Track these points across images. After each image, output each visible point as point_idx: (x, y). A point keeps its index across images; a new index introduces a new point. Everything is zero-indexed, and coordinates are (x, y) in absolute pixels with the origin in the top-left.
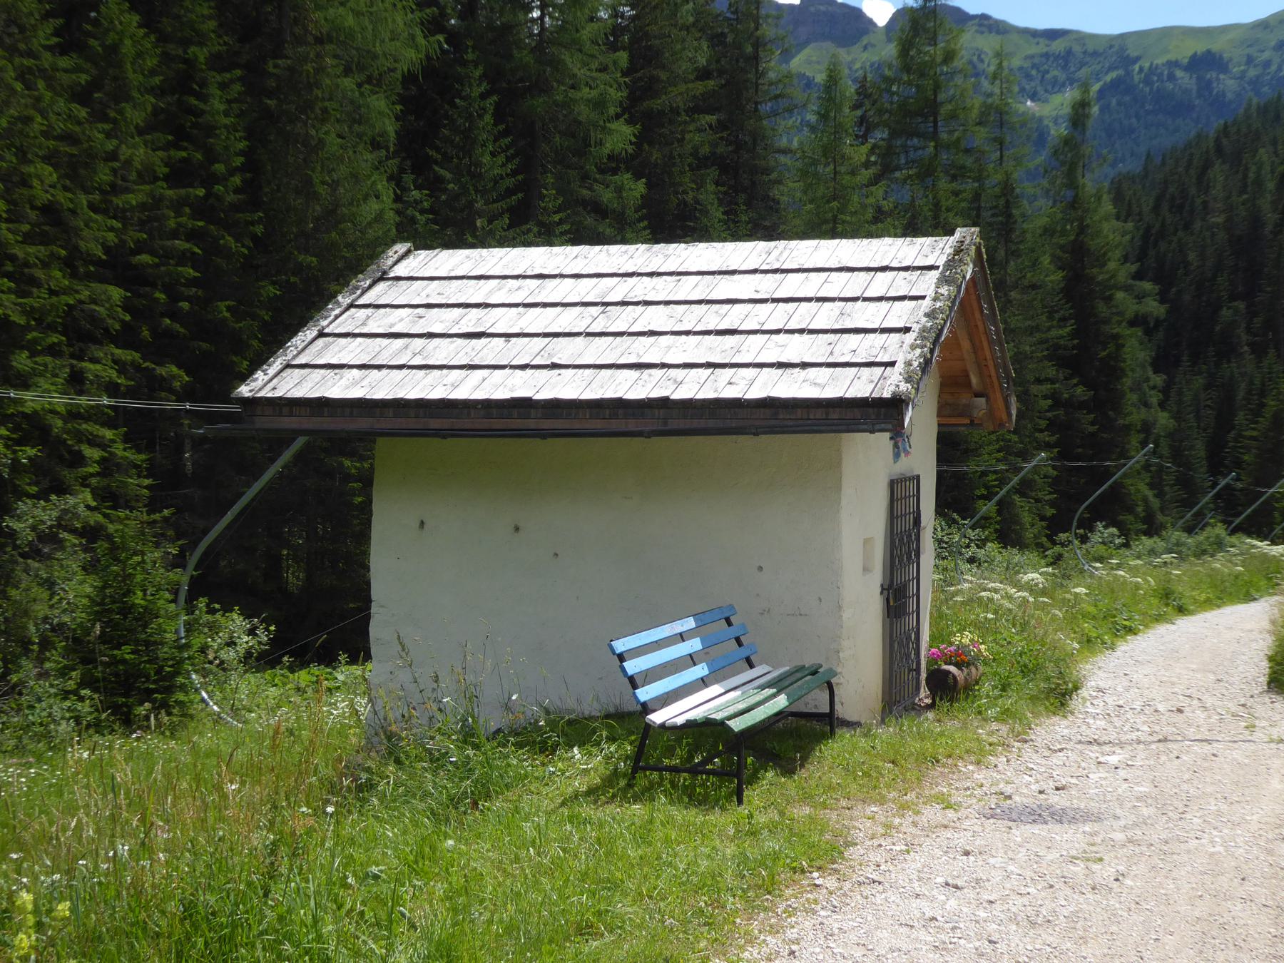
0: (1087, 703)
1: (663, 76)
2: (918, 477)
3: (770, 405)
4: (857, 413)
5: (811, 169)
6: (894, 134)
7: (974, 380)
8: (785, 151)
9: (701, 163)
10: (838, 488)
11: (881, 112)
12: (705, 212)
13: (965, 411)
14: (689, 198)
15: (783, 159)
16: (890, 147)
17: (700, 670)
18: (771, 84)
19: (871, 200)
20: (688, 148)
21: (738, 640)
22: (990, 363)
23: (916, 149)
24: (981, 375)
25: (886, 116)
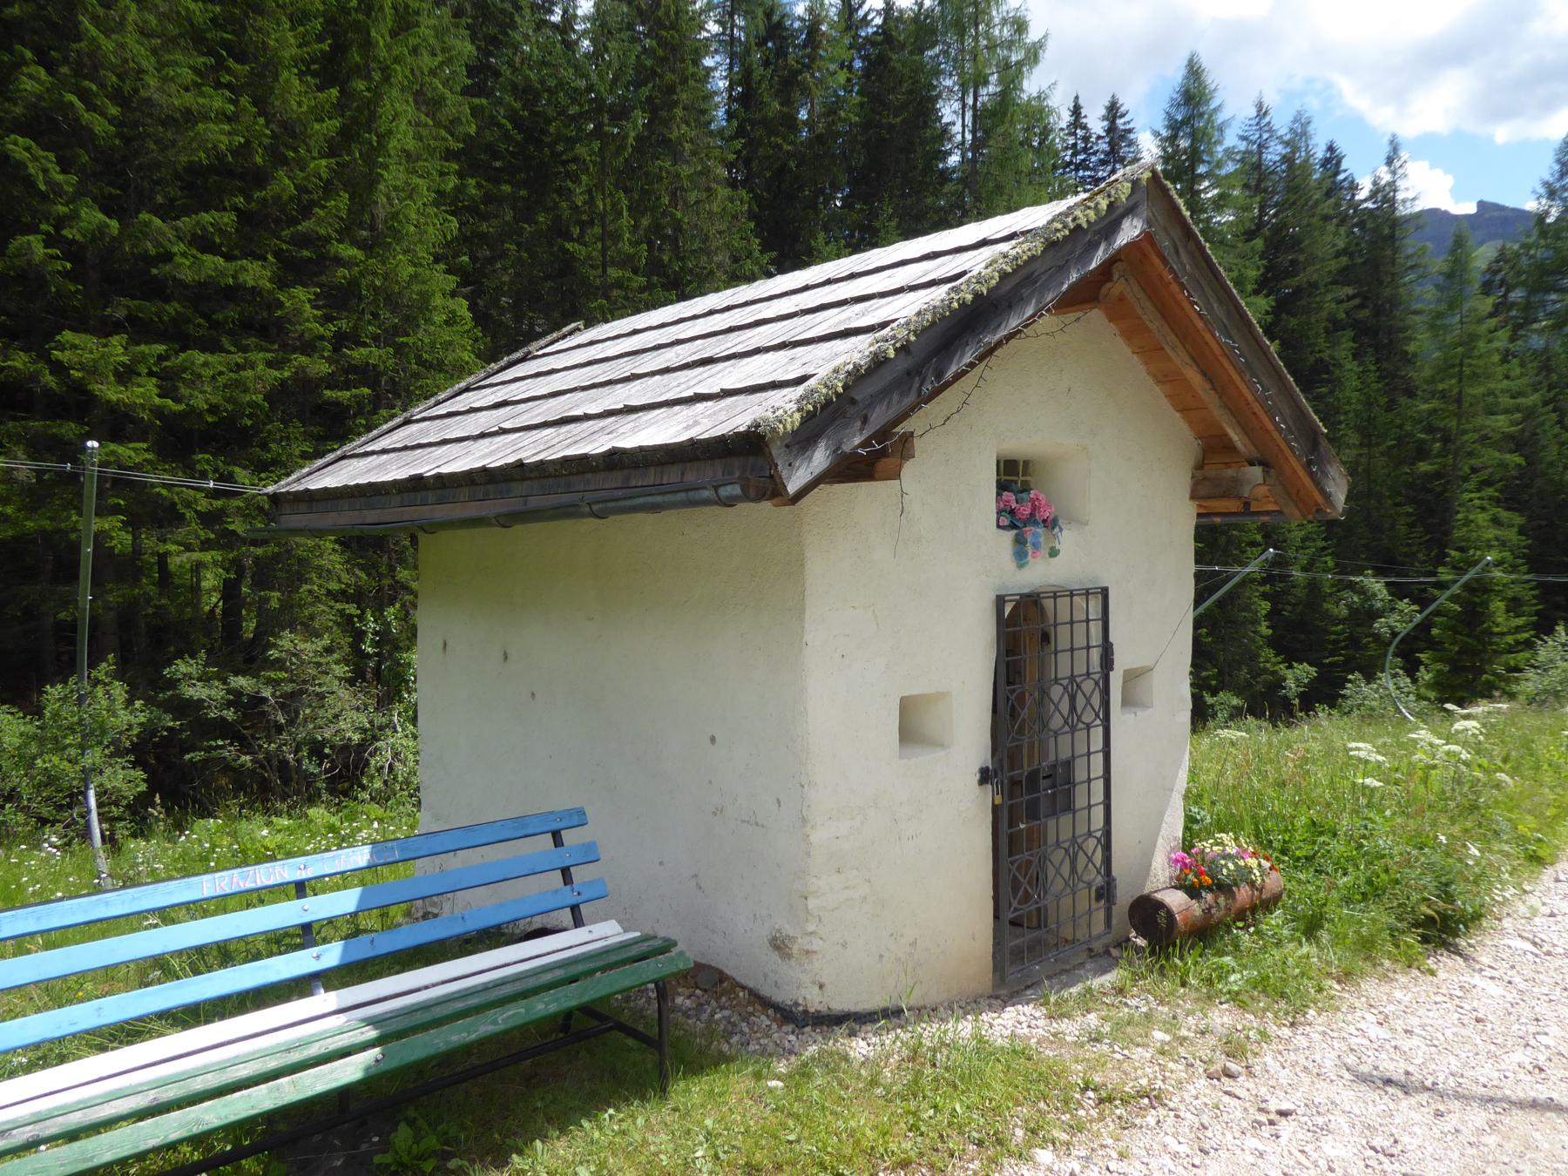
0: (1500, 946)
1: (1302, 258)
2: (1105, 592)
3: (616, 459)
4: (711, 471)
5: (1439, 322)
6: (1532, 291)
7: (1235, 436)
8: (1417, 312)
9: (1335, 326)
10: (800, 611)
11: (1519, 273)
12: (1339, 365)
13: (1229, 490)
14: (1325, 355)
15: (1417, 318)
16: (1529, 303)
17: (330, 955)
18: (1408, 257)
19: (1496, 344)
20: (1324, 314)
21: (566, 873)
22: (1256, 407)
23: (1555, 302)
24: (1246, 429)
25: (1523, 277)
